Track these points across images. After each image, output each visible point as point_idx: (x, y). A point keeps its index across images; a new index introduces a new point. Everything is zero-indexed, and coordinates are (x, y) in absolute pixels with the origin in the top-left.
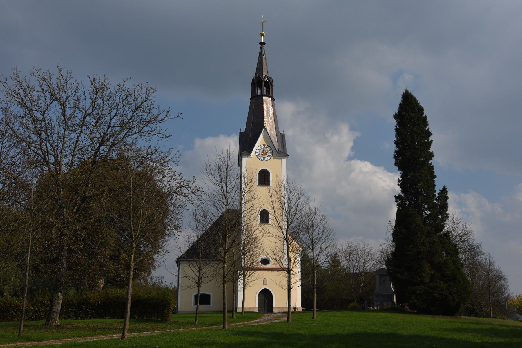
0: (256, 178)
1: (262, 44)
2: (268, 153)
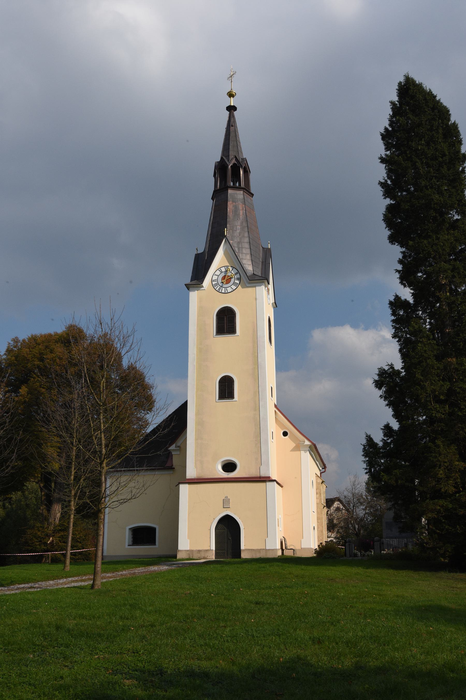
0: (212, 323)
1: (231, 109)
2: (232, 280)
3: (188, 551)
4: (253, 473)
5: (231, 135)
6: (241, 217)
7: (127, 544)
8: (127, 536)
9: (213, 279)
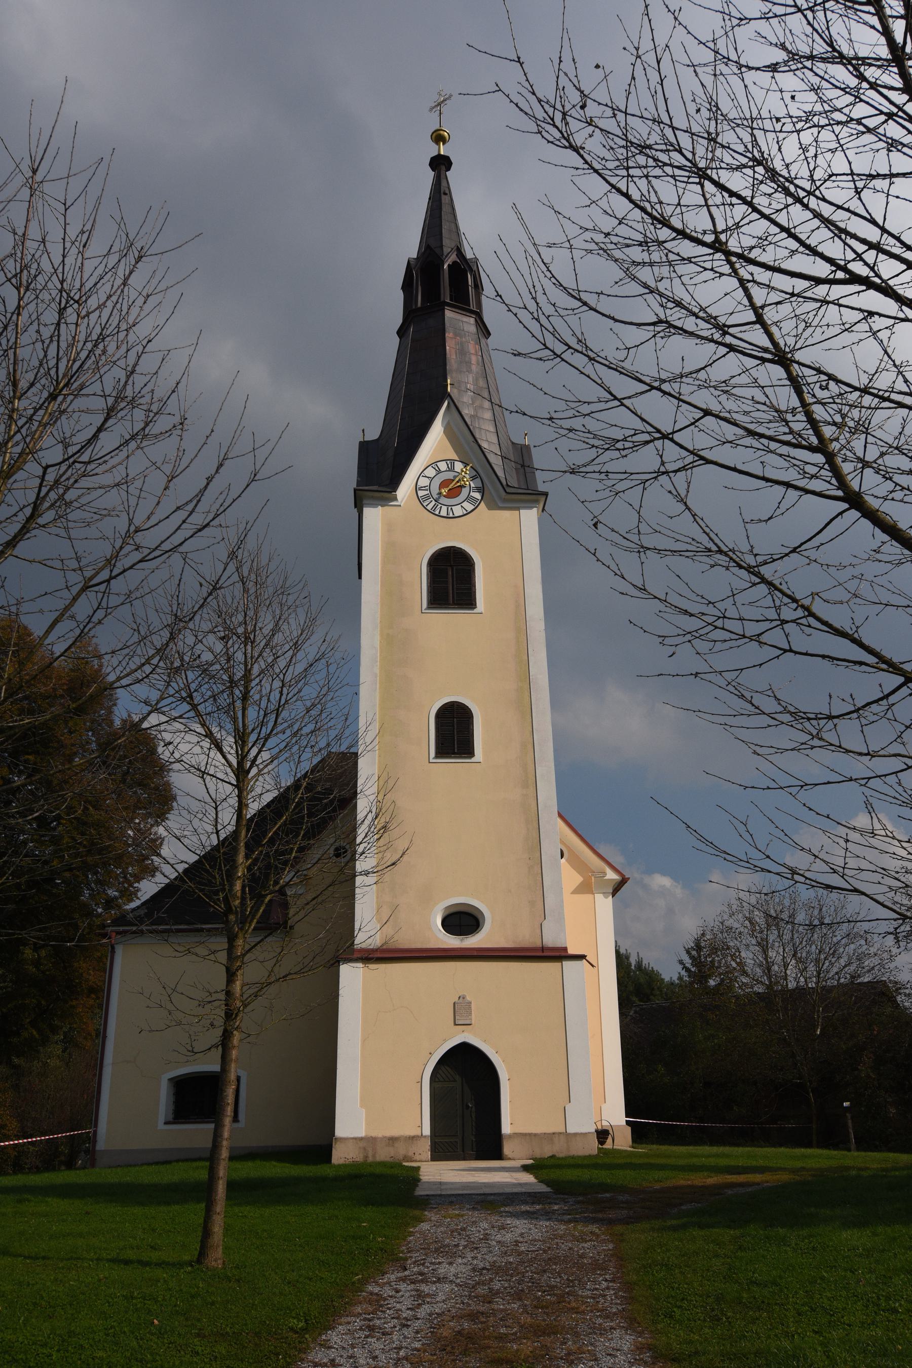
2: (465, 492)
3: (361, 1139)
4: (525, 938)
5: (444, 209)
6: (474, 368)
7: (161, 1119)
8: (163, 1099)
9: (420, 484)
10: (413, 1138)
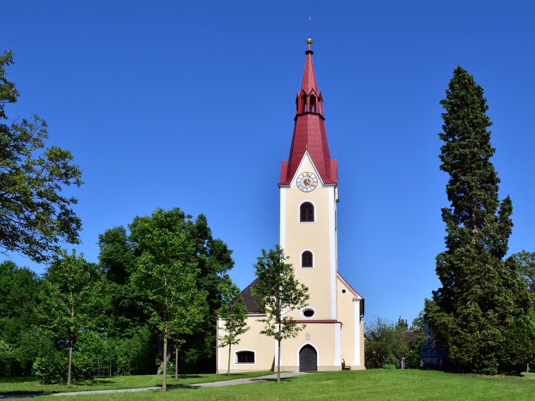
10: (294, 367)
